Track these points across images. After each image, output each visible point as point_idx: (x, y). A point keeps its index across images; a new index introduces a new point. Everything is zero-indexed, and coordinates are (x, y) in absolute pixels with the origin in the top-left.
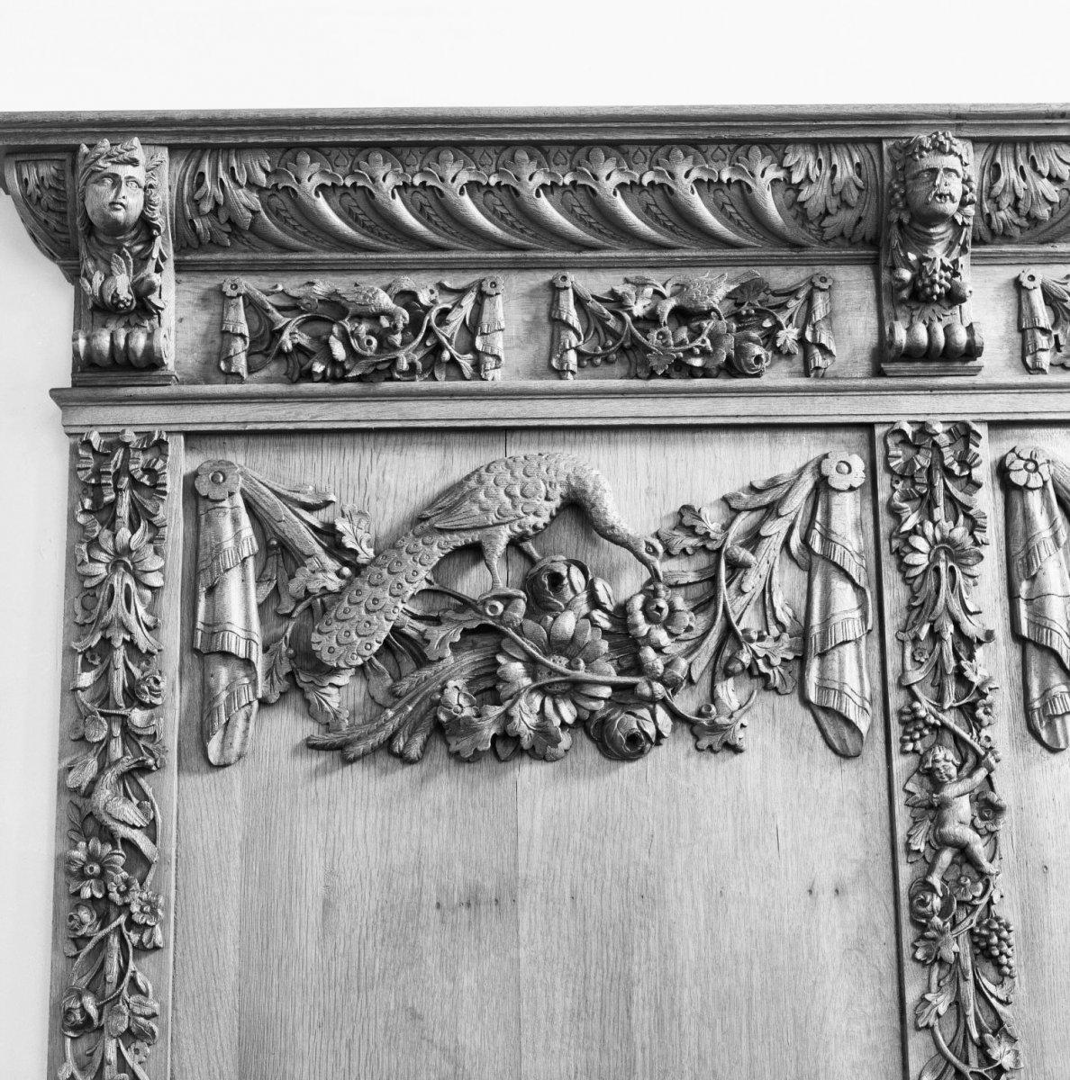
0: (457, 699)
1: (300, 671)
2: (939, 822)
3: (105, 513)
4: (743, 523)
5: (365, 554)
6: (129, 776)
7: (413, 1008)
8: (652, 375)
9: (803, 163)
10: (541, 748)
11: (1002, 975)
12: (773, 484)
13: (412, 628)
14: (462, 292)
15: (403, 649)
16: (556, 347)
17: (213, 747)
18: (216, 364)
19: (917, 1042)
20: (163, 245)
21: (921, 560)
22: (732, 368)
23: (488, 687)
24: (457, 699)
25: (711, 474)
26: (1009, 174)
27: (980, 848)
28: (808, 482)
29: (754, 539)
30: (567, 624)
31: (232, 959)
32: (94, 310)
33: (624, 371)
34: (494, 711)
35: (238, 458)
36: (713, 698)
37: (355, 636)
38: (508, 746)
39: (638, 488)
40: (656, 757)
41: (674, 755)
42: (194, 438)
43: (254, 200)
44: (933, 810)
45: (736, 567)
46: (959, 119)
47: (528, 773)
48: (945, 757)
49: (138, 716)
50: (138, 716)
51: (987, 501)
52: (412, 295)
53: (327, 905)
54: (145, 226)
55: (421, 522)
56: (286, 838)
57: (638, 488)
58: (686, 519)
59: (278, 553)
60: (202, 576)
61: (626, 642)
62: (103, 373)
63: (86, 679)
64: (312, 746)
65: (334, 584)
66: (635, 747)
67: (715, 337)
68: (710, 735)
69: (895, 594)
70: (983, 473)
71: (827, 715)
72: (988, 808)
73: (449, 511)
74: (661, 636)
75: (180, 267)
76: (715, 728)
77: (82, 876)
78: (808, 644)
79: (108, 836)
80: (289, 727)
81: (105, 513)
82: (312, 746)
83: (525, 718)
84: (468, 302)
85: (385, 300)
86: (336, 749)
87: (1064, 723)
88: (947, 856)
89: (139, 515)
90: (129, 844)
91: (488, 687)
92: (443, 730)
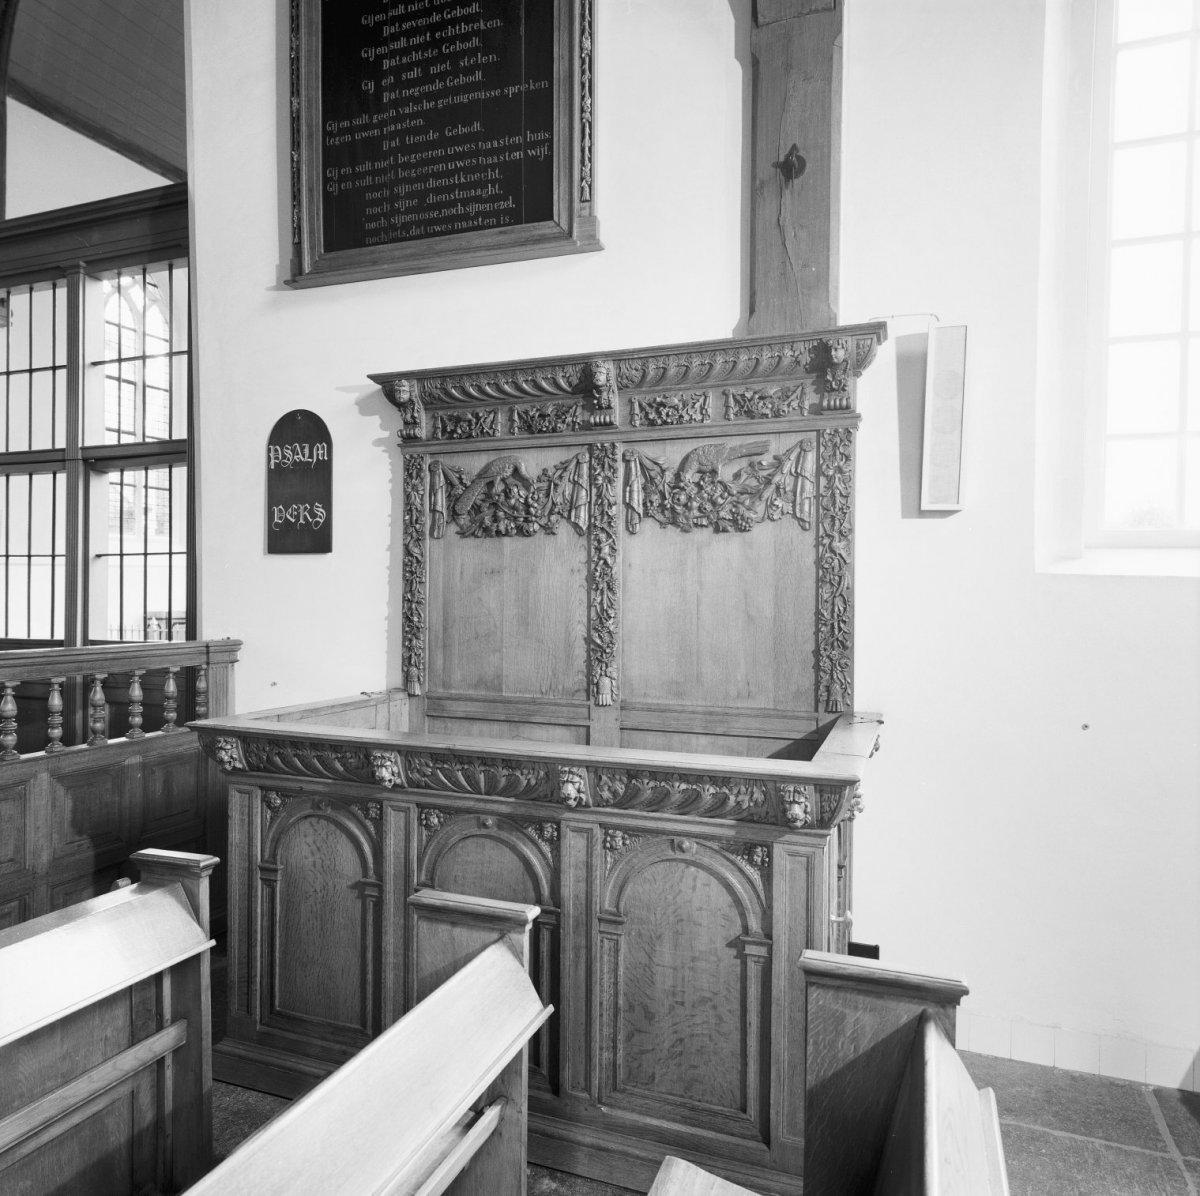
0: (488, 521)
1: (454, 515)
2: (600, 553)
3: (410, 475)
4: (559, 472)
5: (469, 483)
6: (418, 540)
7: (235, 1114)
8: (533, 433)
9: (570, 370)
10: (507, 534)
11: (614, 594)
12: (566, 462)
13: (479, 502)
14: (490, 412)
15: (477, 509)
16: (512, 427)
17: (435, 534)
18: (434, 436)
19: (593, 609)
20: (419, 405)
21: (600, 482)
22: (554, 430)
23: (496, 519)
24: (488, 521)
25: (551, 459)
26: (624, 370)
27: (609, 561)
28: (575, 461)
29: (561, 477)
30: (513, 501)
31: (441, 585)
32: (406, 423)
33: (518, 1078)
34: (496, 524)
35: (441, 459)
36: (549, 520)
37: (465, 506)
38: (498, 533)
39: (532, 463)
40: (537, 536)
41: (541, 535)
42: (432, 454)
43: (438, 392)
44: (599, 550)
45: (556, 485)
46: (606, 356)
47: (506, 540)
48: (603, 536)
49: (418, 526)
50: (418, 526)
51: (621, 467)
52: (477, 414)
53: (462, 573)
54: (411, 401)
55: (480, 476)
56: (455, 557)
57: (532, 463)
58: (545, 471)
59: (450, 484)
60: (433, 491)
61: (527, 505)
62: (408, 440)
63: (407, 517)
64: (457, 533)
65: (460, 491)
66: (528, 534)
67: (550, 422)
68: (549, 530)
69: (594, 491)
70: (619, 457)
71: (576, 526)
72: (613, 549)
73: (486, 472)
74: (536, 505)
75: (426, 409)
76: (549, 528)
77: (407, 565)
78: (572, 505)
79: (412, 556)
80: (453, 528)
81: (410, 475)
82: (457, 533)
83: (502, 528)
84: (492, 416)
85: (470, 416)
86: (462, 534)
87: (149, 437)
88: (602, 562)
89: (418, 475)
90: (416, 558)
91: (496, 519)
92: (486, 531)
